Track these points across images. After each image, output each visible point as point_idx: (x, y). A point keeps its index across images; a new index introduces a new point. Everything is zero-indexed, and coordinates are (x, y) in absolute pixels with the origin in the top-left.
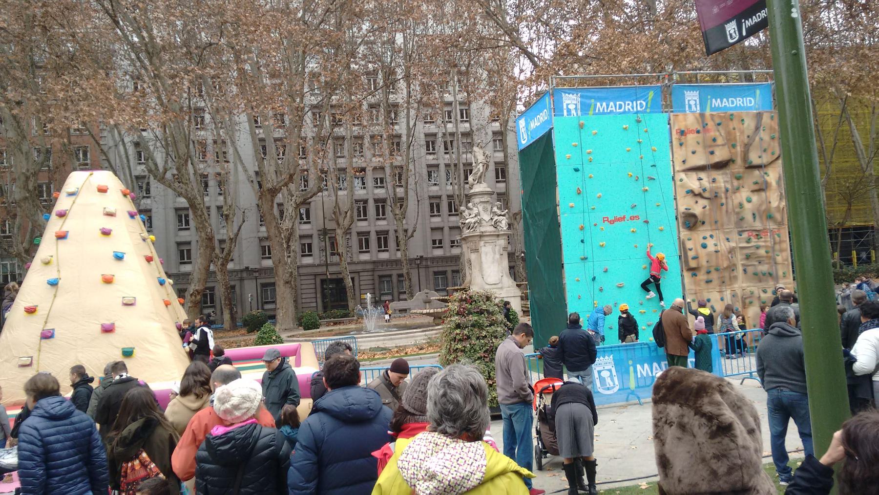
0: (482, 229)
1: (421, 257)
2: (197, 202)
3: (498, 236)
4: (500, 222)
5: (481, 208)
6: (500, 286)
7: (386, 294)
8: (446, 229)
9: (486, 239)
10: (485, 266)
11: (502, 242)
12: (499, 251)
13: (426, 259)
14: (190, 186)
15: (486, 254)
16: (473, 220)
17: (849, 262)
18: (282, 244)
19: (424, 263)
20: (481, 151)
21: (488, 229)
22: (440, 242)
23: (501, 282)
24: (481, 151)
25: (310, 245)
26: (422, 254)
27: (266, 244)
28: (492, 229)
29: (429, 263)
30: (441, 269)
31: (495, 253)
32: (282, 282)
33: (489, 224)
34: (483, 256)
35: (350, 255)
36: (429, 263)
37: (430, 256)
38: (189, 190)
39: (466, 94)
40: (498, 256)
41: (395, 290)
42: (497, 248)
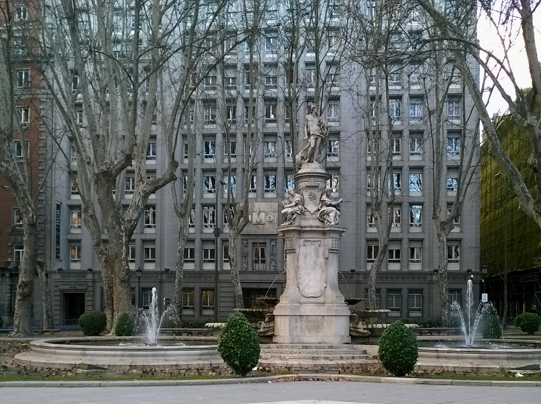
0: (304, 223)
1: (353, 271)
2: (19, 183)
3: (324, 233)
4: (328, 214)
5: (306, 195)
6: (321, 300)
10: (302, 272)
12: (324, 252)
13: (358, 274)
14: (12, 164)
15: (306, 257)
16: (290, 210)
18: (121, 237)
19: (355, 277)
20: (316, 120)
21: (311, 222)
23: (323, 293)
24: (316, 120)
26: (353, 268)
29: (361, 279)
30: (416, 286)
31: (317, 256)
32: (118, 280)
33: (314, 216)
34: (301, 258)
35: (273, 264)
36: (361, 279)
37: (363, 270)
38: (10, 168)
40: (321, 260)
41: (405, 305)
42: (321, 249)
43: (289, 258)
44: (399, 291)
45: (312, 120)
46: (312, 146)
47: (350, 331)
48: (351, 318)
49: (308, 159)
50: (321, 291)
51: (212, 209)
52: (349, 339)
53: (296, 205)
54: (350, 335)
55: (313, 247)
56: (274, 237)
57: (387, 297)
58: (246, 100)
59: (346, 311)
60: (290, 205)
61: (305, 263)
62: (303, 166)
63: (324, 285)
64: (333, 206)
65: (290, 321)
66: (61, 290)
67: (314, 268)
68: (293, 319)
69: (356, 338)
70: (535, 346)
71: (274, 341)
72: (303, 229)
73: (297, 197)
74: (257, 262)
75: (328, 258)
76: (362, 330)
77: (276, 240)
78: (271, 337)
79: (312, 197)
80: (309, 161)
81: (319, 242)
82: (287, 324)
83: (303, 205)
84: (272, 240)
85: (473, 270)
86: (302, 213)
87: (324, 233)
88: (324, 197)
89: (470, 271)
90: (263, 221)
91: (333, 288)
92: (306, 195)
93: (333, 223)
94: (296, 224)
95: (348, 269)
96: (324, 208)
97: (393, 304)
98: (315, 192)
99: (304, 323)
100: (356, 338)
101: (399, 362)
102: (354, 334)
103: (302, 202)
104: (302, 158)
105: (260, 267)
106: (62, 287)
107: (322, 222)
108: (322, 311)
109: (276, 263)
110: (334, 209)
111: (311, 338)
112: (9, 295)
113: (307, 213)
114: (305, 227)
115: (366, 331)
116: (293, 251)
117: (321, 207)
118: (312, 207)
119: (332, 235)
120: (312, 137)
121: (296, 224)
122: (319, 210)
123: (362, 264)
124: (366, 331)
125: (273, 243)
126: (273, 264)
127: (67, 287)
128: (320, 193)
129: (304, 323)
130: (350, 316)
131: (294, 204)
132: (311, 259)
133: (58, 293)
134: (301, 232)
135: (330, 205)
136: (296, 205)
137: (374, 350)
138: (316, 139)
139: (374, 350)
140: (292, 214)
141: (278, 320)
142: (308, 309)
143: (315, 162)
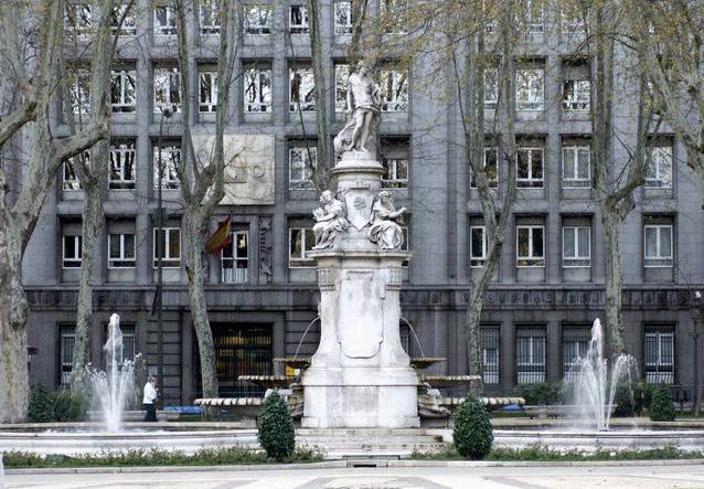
6: (373, 362)
11: (388, 274)
12: (377, 292)
15: (351, 296)
21: (358, 244)
28: (370, 246)
34: (344, 299)
35: (266, 269)
40: (374, 302)
45: (359, 85)
46: (359, 125)
47: (419, 408)
48: (421, 390)
49: (352, 144)
51: (123, 149)
52: (417, 422)
54: (419, 415)
55: (361, 282)
57: (515, 339)
59: (412, 378)
60: (325, 218)
62: (345, 156)
64: (393, 219)
67: (363, 312)
68: (332, 390)
69: (427, 419)
70: (698, 427)
71: (304, 425)
72: (347, 255)
73: (336, 206)
75: (383, 299)
76: (435, 408)
77: (271, 216)
79: (360, 205)
81: (370, 275)
86: (345, 230)
87: (378, 259)
88: (378, 206)
92: (351, 199)
96: (378, 222)
97: (528, 356)
98: (363, 195)
101: (473, 446)
102: (424, 413)
103: (345, 213)
104: (344, 142)
107: (375, 243)
109: (271, 268)
110: (393, 224)
111: (357, 418)
113: (352, 229)
115: (442, 409)
117: (373, 220)
118: (359, 220)
119: (390, 263)
122: (370, 225)
124: (442, 409)
125: (265, 224)
126: (266, 269)
128: (372, 198)
130: (418, 386)
131: (332, 215)
132: (359, 298)
135: (387, 218)
139: (448, 435)
140: (330, 232)
141: (308, 391)
142: (352, 377)
143: (362, 148)
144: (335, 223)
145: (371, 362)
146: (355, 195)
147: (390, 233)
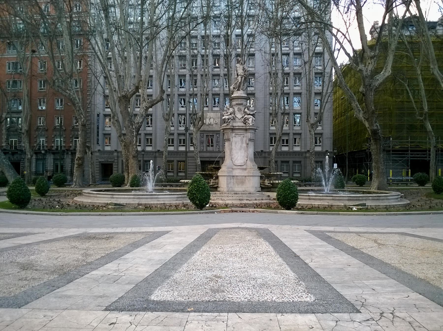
0: (235, 124)
1: (262, 151)
3: (246, 130)
4: (248, 119)
5: (236, 109)
6: (244, 167)
7: (296, 173)
8: (291, 135)
9: (236, 131)
15: (236, 143)
16: (227, 117)
17: (22, 49)
19: (263, 155)
20: (241, 67)
22: (287, 141)
23: (245, 164)
24: (241, 67)
25: (173, 140)
26: (262, 149)
27: (149, 137)
28: (242, 124)
30: (297, 160)
31: (242, 143)
33: (240, 121)
34: (233, 144)
35: (218, 147)
37: (268, 151)
39: (241, 30)
40: (245, 145)
41: (291, 170)
42: (245, 139)
43: (227, 144)
44: (288, 162)
46: (240, 81)
50: (244, 162)
53: (230, 114)
54: (261, 187)
56: (218, 132)
58: (203, 56)
61: (235, 146)
63: (246, 159)
64: (251, 115)
65: (227, 179)
66: (100, 162)
74: (208, 146)
78: (217, 188)
79: (240, 110)
80: (238, 90)
82: (225, 181)
83: (234, 114)
84: (217, 134)
85: (329, 151)
89: (327, 151)
90: (212, 123)
91: (251, 161)
93: (251, 125)
94: (230, 125)
95: (259, 150)
99: (235, 180)
100: (264, 188)
103: (234, 113)
105: (210, 149)
106: (100, 160)
108: (245, 173)
110: (252, 116)
112: (71, 164)
114: (235, 126)
115: (269, 185)
116: (229, 140)
118: (239, 115)
120: (239, 77)
121: (230, 125)
122: (243, 117)
123: (267, 147)
124: (269, 185)
127: (103, 160)
129: (235, 180)
131: (229, 114)
133: (98, 163)
134: (233, 129)
135: (249, 114)
136: (230, 114)
137: (274, 195)
138: (242, 77)
141: (220, 178)
144: (230, 116)
145: (242, 167)
146: (238, 107)
147: (250, 120)
